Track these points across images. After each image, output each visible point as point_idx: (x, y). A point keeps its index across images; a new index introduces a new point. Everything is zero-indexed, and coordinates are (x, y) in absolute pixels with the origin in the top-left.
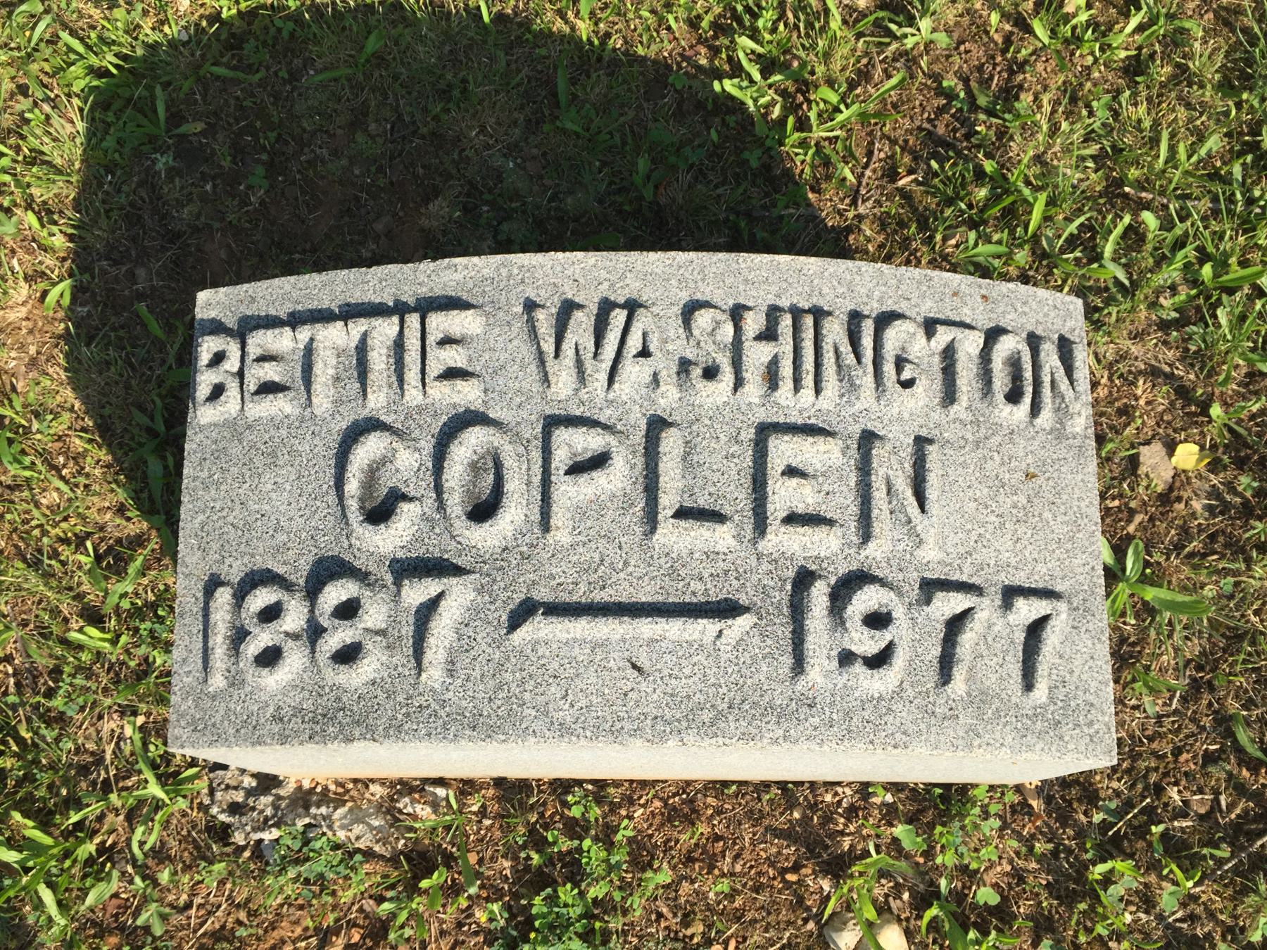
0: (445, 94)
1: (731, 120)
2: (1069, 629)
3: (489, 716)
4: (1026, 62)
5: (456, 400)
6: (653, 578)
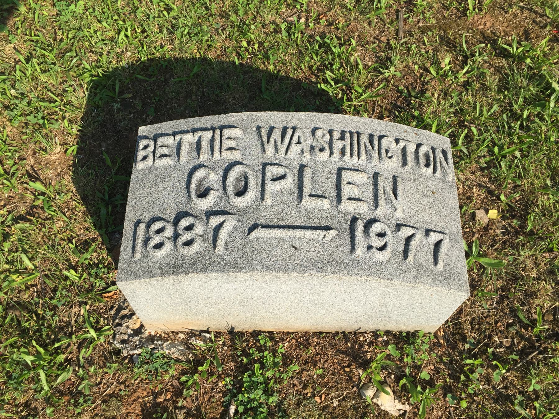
0: (221, 87)
1: (324, 98)
2: (450, 246)
3: (240, 264)
4: (428, 82)
5: (232, 158)
6: (301, 218)
